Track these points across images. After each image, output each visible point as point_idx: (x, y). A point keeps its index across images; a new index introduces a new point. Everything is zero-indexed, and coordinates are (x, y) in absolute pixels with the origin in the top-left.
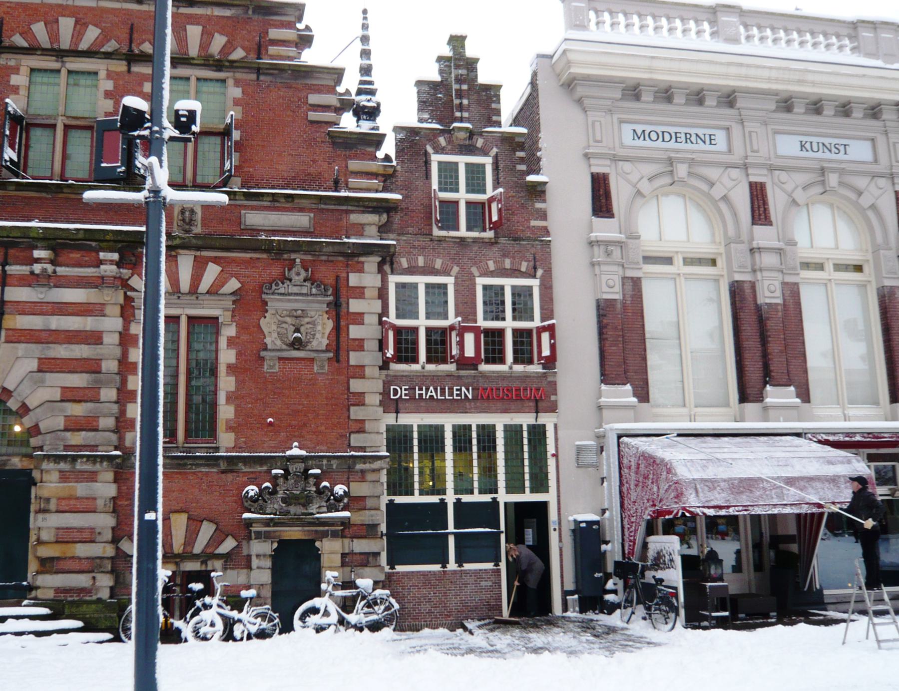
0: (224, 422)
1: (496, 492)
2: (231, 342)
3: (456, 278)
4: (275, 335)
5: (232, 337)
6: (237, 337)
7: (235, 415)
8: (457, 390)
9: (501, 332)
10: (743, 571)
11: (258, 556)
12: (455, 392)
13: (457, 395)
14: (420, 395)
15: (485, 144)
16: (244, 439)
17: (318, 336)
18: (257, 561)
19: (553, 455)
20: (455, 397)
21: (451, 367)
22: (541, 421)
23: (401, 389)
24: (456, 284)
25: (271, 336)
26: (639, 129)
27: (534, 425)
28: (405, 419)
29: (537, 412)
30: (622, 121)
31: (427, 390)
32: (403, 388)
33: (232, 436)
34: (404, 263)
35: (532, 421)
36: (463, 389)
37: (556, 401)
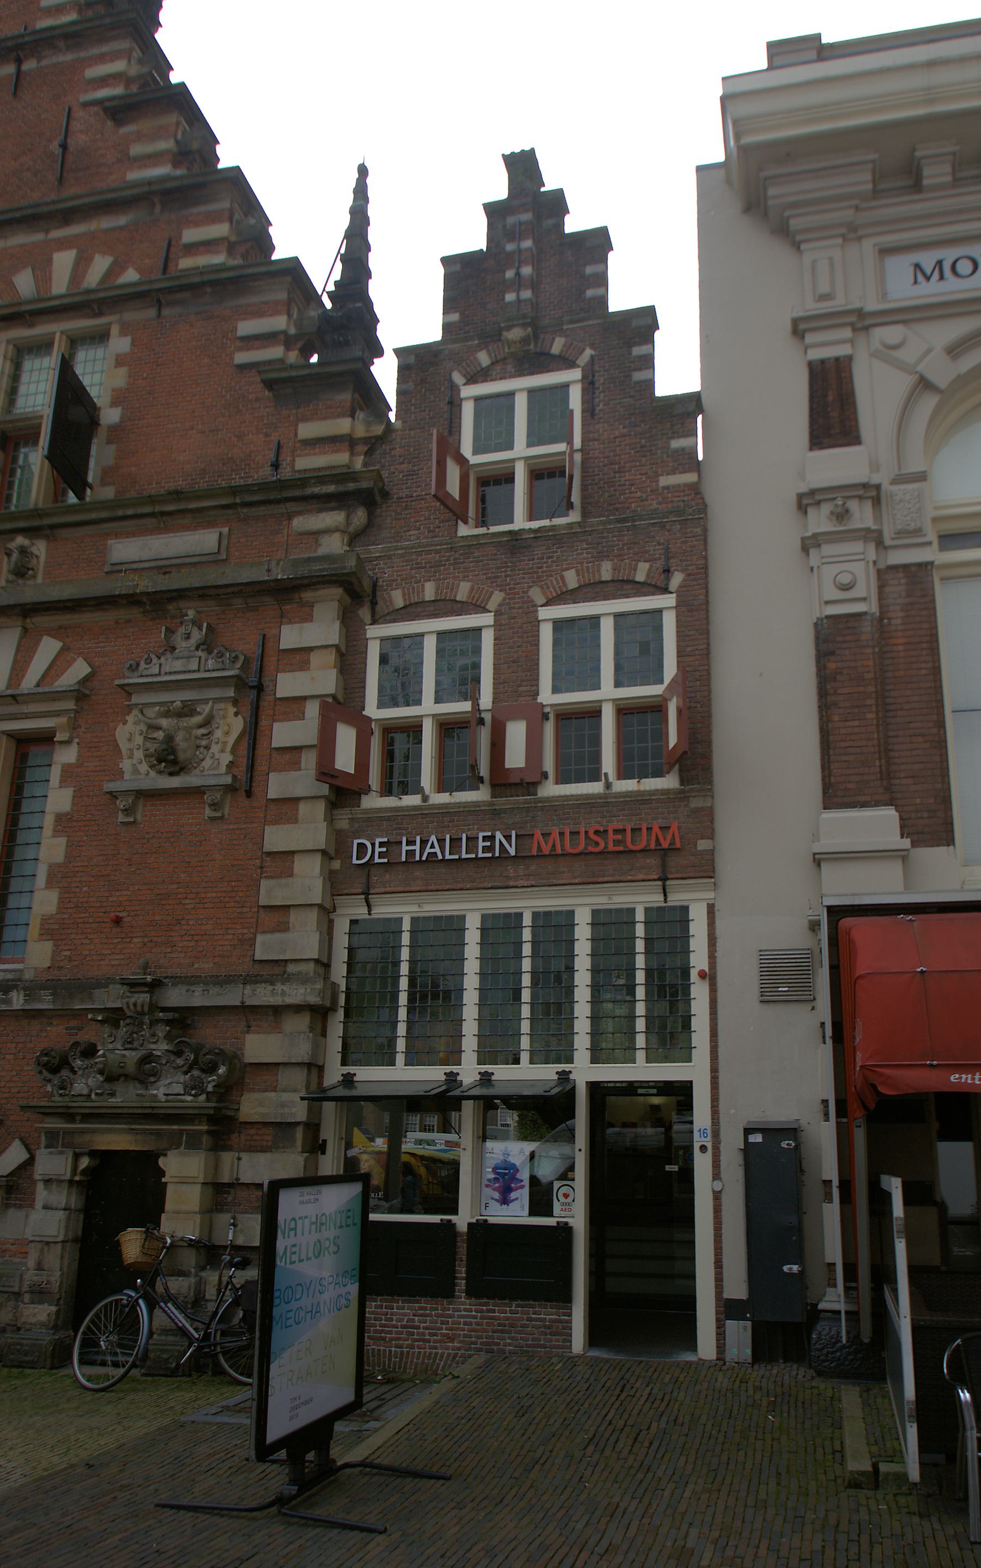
0: (38, 921)
1: (570, 1060)
2: (68, 774)
3: (498, 614)
4: (139, 754)
5: (70, 765)
6: (79, 764)
7: (59, 908)
8: (485, 839)
9: (593, 713)
10: (528, 449)
11: (48, 1182)
12: (481, 844)
13: (485, 849)
14: (410, 853)
15: (567, 346)
16: (68, 953)
17: (215, 749)
18: (45, 1193)
19: (702, 975)
20: (481, 855)
21: (480, 795)
22: (676, 898)
23: (373, 845)
24: (497, 626)
25: (131, 757)
26: (928, 260)
27: (659, 909)
28: (385, 909)
29: (664, 879)
30: (885, 252)
31: (424, 843)
32: (377, 841)
33: (48, 946)
34: (398, 599)
35: (656, 899)
36: (499, 836)
37: (712, 852)
